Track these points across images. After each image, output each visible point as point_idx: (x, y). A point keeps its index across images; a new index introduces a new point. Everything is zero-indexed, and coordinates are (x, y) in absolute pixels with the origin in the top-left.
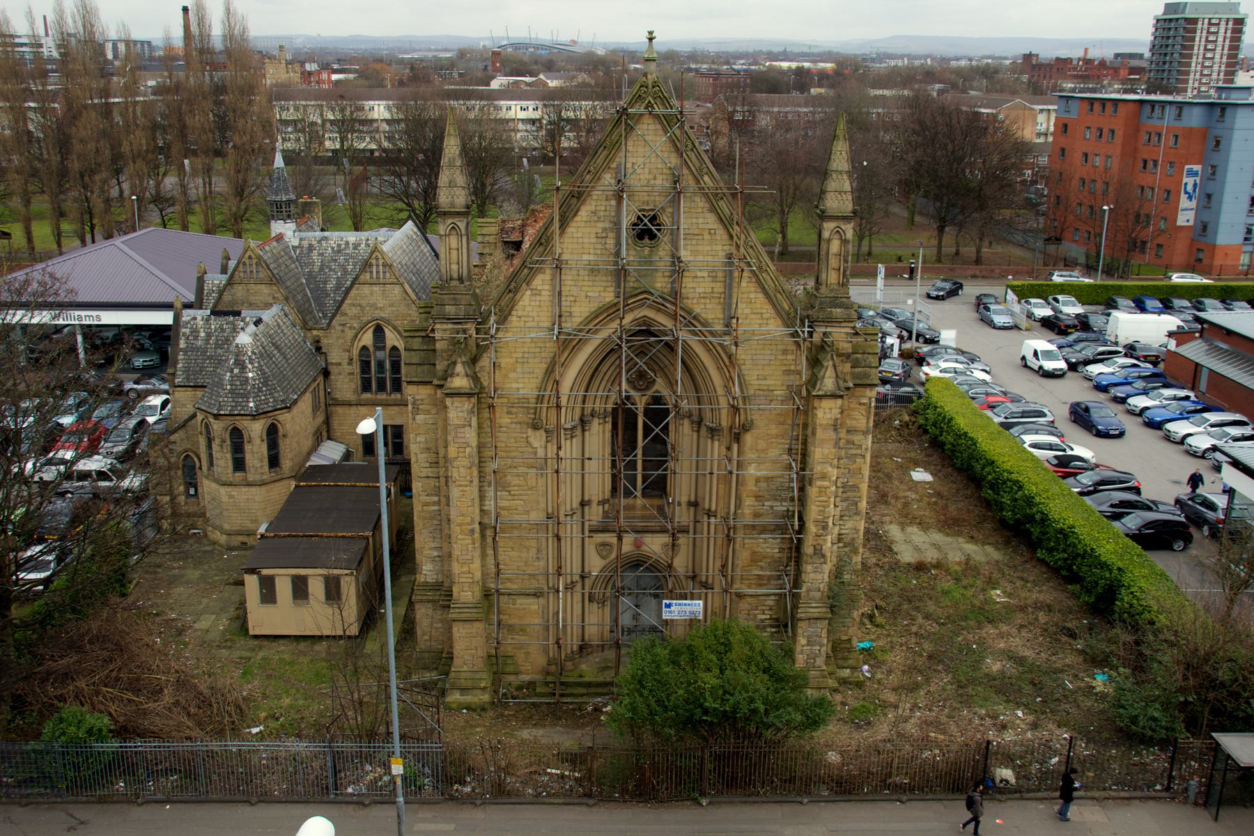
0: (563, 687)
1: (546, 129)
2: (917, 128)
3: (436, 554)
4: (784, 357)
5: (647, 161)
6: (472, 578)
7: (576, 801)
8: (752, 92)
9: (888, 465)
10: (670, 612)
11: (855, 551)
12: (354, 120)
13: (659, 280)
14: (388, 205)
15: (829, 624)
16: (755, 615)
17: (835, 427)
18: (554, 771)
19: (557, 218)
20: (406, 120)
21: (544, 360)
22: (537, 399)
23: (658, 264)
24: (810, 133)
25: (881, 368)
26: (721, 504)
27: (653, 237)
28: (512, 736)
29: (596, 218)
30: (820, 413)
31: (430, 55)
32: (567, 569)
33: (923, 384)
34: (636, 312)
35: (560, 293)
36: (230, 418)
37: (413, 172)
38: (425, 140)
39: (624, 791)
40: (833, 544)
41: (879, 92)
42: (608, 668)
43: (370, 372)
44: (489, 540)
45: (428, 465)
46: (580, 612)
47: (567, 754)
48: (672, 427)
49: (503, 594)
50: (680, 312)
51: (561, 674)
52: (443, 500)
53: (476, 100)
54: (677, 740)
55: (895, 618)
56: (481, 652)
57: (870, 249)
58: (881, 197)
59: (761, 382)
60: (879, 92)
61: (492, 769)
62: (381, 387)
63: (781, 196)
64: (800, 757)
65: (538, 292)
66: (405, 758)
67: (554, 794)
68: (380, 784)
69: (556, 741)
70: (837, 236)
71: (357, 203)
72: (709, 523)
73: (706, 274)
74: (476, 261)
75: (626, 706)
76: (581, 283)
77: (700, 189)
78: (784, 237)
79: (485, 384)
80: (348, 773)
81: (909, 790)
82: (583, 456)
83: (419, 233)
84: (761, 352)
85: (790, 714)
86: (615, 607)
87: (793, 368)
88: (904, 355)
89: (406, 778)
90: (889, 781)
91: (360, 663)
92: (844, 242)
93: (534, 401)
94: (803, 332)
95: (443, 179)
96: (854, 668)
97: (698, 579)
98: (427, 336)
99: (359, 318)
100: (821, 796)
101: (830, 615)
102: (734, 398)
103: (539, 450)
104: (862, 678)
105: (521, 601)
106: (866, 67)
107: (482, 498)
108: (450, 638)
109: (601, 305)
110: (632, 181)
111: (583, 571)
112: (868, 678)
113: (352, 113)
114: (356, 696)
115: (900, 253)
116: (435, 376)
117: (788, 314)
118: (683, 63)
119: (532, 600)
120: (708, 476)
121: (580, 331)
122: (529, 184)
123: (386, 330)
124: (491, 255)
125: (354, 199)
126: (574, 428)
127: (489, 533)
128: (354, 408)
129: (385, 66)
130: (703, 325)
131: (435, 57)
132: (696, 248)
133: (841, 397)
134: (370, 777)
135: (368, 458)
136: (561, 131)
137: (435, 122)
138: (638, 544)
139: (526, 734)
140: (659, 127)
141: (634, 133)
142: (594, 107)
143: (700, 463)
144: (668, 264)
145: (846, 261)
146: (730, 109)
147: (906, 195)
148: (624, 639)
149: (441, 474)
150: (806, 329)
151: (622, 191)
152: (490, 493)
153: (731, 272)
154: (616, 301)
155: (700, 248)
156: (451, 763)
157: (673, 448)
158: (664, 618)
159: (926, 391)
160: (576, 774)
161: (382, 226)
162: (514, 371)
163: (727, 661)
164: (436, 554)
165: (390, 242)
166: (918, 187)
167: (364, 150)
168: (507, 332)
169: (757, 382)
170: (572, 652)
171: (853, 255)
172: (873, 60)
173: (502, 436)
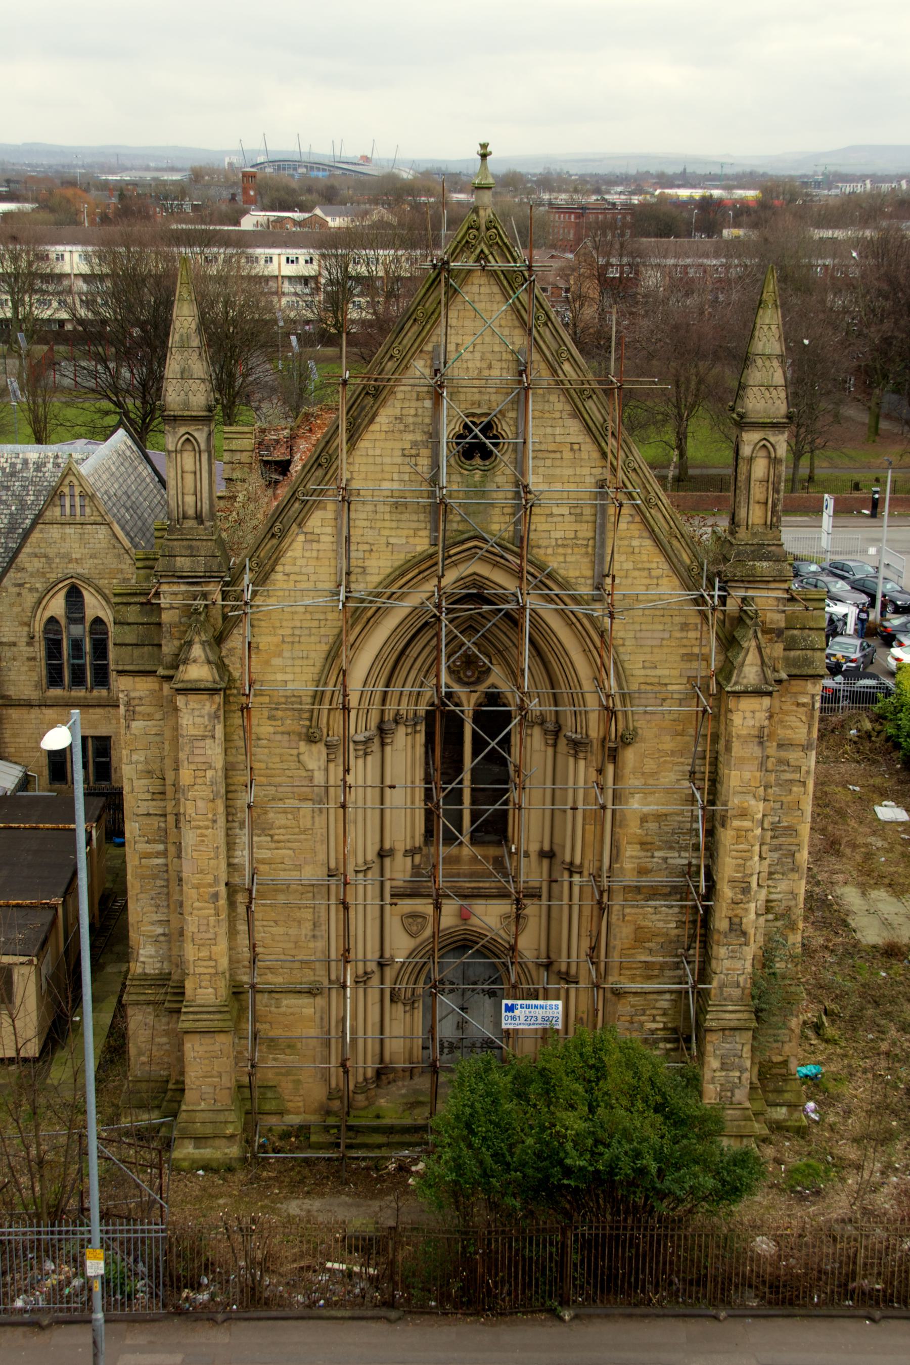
0: (350, 1134)
1: (325, 292)
2: (885, 287)
3: (160, 930)
4: (684, 634)
5: (479, 341)
6: (215, 967)
7: (370, 1313)
8: (633, 236)
9: (840, 795)
10: (513, 1018)
11: (792, 927)
12: (33, 275)
13: (496, 519)
14: (87, 405)
15: (754, 1038)
16: (642, 1024)
17: (761, 739)
18: (336, 1266)
19: (343, 426)
20: (113, 276)
21: (324, 640)
22: (314, 697)
23: (494, 495)
24: (721, 297)
25: (828, 651)
26: (589, 856)
27: (486, 454)
28: (274, 1211)
29: (402, 427)
31: (148, 176)
32: (358, 952)
33: (892, 674)
34: (462, 568)
35: (348, 539)
37: (126, 355)
38: (143, 307)
39: (444, 1297)
40: (758, 915)
41: (828, 233)
42: (418, 1104)
43: (60, 657)
44: (241, 909)
45: (149, 797)
46: (377, 1018)
47: (357, 1238)
48: (515, 740)
49: (261, 991)
50: (527, 567)
51: (348, 1114)
52: (172, 849)
53: (220, 246)
54: (525, 1217)
55: (855, 1030)
56: (228, 1081)
57: (812, 471)
58: (829, 393)
59: (649, 672)
60: (828, 233)
61: (243, 1264)
62: (78, 679)
63: (678, 393)
64: (712, 1244)
65: (315, 538)
66: (108, 1249)
67: (336, 1303)
68: (67, 1291)
69: (340, 1218)
70: (763, 453)
71: (40, 400)
72: (571, 883)
73: (565, 511)
74: (221, 490)
75: (446, 1162)
76: (379, 524)
77: (558, 383)
78: (682, 455)
79: (236, 674)
80: (17, 1276)
81: (885, 1301)
82: (382, 782)
83: (135, 448)
84: (650, 627)
85: (696, 1176)
86: (430, 1010)
87: (696, 650)
88: (866, 630)
89: (108, 1281)
90: (851, 1286)
91: (41, 1101)
92: (774, 461)
93: (309, 700)
94: (712, 597)
95: (172, 367)
96: (793, 1106)
97: (555, 968)
98: (149, 603)
100: (746, 1307)
101: (754, 1024)
102: (608, 696)
103: (316, 774)
104: (805, 1122)
105: (289, 1002)
106: (807, 195)
107: (230, 845)
108: (181, 1059)
109: (409, 556)
110: (459, 371)
111: (382, 956)
112: (815, 1121)
113: (30, 264)
114: (33, 1152)
115: (857, 477)
116: (160, 662)
117: (689, 570)
118: (530, 192)
119: (305, 1000)
120: (570, 812)
121: (378, 595)
122: (301, 375)
123: (85, 593)
124: (243, 481)
125: (34, 394)
126: (369, 740)
127: (241, 898)
128: (35, 712)
129: (79, 192)
130: (561, 586)
131: (155, 179)
132: (550, 472)
133: (770, 694)
134: (52, 1281)
135: (57, 786)
136: (348, 294)
137: (158, 279)
138: (464, 915)
139: (294, 1207)
140: (496, 289)
141: (459, 298)
142: (397, 259)
143: (558, 793)
144: (510, 495)
145: (776, 491)
146: (601, 261)
147: (867, 388)
148: (444, 1060)
149: (169, 810)
150: (717, 593)
151: (441, 386)
152: (243, 837)
153: (604, 508)
154: (431, 551)
155: (558, 471)
156: (178, 1256)
157: (518, 771)
158: (504, 1026)
159: (897, 685)
160: (371, 1271)
161: (78, 437)
162: (280, 654)
163: (600, 1094)
165: (91, 461)
166: (885, 377)
167: (49, 321)
168: (269, 596)
169: (643, 672)
170: (365, 1079)
171: (786, 481)
172: (818, 184)
173: (261, 753)
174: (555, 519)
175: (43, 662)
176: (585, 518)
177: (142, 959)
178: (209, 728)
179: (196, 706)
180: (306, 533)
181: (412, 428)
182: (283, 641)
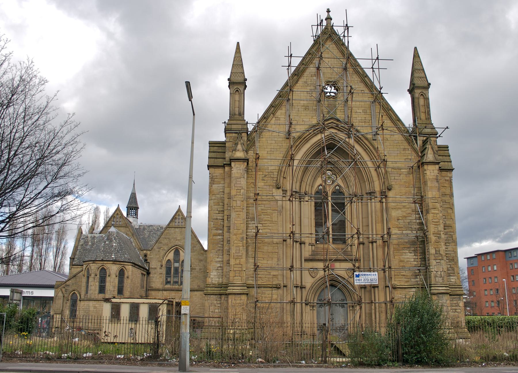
4: (404, 152)
10: (359, 280)
13: (338, 113)
30: (428, 172)
36: (101, 262)
65: (279, 119)
70: (422, 97)
73: (361, 111)
84: (393, 149)
99: (167, 245)
123: (181, 251)
140: (334, 46)
164: (219, 265)
174: (358, 113)
175: (165, 275)
176: (367, 113)
179: (238, 166)
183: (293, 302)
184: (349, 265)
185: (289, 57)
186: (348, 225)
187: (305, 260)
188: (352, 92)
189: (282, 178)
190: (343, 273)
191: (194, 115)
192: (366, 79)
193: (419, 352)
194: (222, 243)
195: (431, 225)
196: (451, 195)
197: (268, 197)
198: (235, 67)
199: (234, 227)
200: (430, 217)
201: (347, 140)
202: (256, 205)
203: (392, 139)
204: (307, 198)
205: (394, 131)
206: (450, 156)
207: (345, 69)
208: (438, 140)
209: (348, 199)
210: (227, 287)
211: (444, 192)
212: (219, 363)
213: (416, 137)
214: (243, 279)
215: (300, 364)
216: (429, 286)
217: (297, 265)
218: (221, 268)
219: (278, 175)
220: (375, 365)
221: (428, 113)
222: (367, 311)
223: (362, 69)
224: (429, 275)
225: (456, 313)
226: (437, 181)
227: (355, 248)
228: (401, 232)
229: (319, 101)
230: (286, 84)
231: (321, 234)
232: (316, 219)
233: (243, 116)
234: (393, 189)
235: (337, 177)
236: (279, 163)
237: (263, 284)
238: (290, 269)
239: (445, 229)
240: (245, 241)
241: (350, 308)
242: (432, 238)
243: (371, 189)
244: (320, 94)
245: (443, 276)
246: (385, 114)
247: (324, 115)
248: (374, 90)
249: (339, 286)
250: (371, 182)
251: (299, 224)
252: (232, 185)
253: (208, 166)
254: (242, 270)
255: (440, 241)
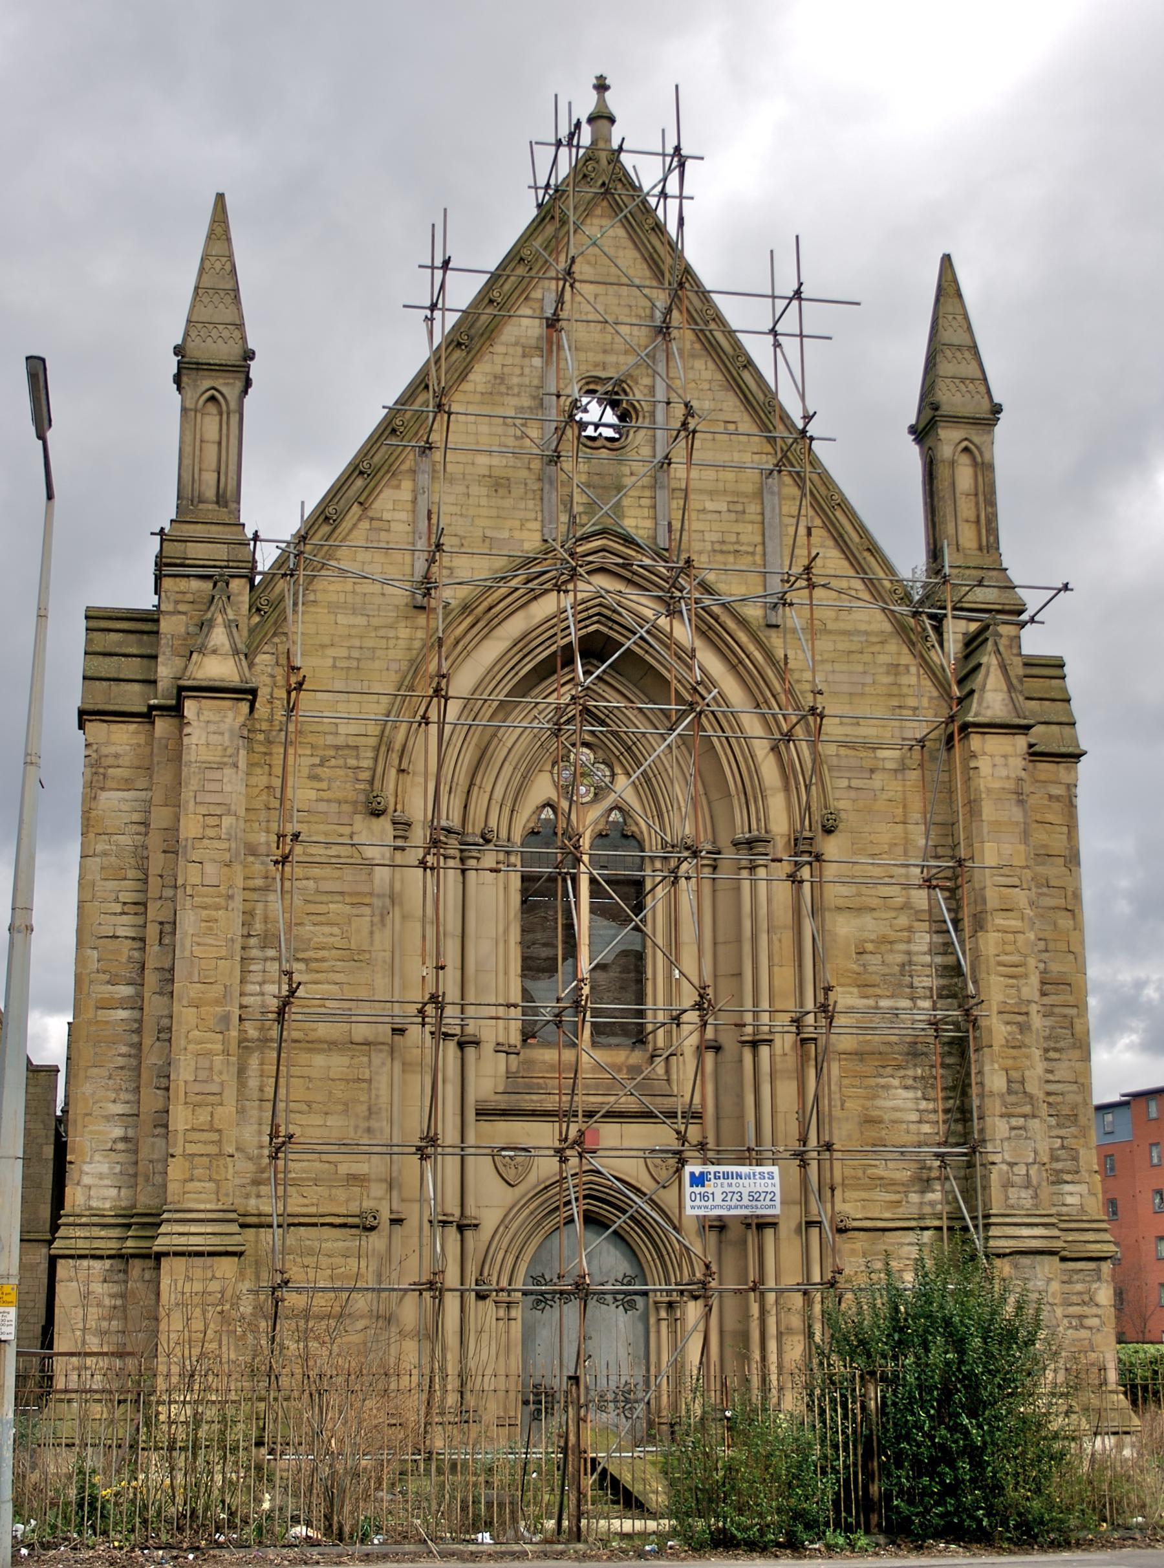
10: (704, 1196)
13: (630, 512)
21: (394, 666)
70: (964, 459)
73: (723, 507)
140: (621, 232)
174: (709, 516)
177: (86, 1180)
178: (229, 751)
180: (372, 519)
181: (516, 391)
182: (334, 667)
183: (433, 1287)
184: (662, 1135)
185: (433, 268)
186: (656, 966)
187: (479, 1113)
188: (691, 427)
189: (393, 772)
190: (633, 1170)
191: (50, 496)
192: (746, 375)
193: (951, 1490)
194: (135, 1038)
195: (994, 979)
196: (1072, 859)
197: (334, 851)
198: (206, 299)
199: (190, 974)
200: (990, 942)
201: (663, 622)
202: (282, 880)
203: (842, 626)
204: (489, 860)
205: (853, 593)
206: (1068, 701)
207: (663, 331)
208: (1027, 634)
209: (658, 865)
210: (159, 1225)
211: (1045, 846)
212: (132, 1550)
213: (938, 622)
214: (222, 1191)
215: (472, 1548)
216: (981, 1222)
217: (449, 1134)
218: (130, 1146)
219: (376, 759)
220: (779, 1545)
221: (988, 526)
222: (731, 1324)
223: (731, 333)
224: (984, 1177)
225: (1084, 1333)
226: (1020, 798)
227: (685, 1068)
228: (871, 1002)
229: (555, 459)
230: (420, 383)
231: (547, 1009)
232: (525, 944)
233: (233, 506)
234: (841, 826)
235: (613, 775)
236: (381, 709)
237: (304, 1210)
238: (419, 1149)
239: (1043, 994)
240: (234, 1033)
241: (657, 1310)
242: (997, 1029)
243: (754, 825)
244: (560, 432)
245: (1034, 1182)
246: (818, 522)
247: (573, 517)
248: (777, 422)
249: (620, 1221)
250: (752, 793)
251: (459, 965)
252: (187, 794)
253: (82, 713)
254: (220, 1154)
255: (1027, 1041)
